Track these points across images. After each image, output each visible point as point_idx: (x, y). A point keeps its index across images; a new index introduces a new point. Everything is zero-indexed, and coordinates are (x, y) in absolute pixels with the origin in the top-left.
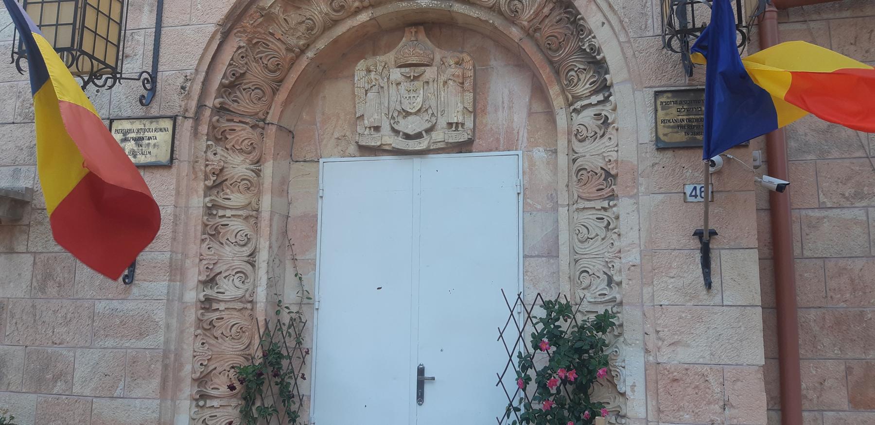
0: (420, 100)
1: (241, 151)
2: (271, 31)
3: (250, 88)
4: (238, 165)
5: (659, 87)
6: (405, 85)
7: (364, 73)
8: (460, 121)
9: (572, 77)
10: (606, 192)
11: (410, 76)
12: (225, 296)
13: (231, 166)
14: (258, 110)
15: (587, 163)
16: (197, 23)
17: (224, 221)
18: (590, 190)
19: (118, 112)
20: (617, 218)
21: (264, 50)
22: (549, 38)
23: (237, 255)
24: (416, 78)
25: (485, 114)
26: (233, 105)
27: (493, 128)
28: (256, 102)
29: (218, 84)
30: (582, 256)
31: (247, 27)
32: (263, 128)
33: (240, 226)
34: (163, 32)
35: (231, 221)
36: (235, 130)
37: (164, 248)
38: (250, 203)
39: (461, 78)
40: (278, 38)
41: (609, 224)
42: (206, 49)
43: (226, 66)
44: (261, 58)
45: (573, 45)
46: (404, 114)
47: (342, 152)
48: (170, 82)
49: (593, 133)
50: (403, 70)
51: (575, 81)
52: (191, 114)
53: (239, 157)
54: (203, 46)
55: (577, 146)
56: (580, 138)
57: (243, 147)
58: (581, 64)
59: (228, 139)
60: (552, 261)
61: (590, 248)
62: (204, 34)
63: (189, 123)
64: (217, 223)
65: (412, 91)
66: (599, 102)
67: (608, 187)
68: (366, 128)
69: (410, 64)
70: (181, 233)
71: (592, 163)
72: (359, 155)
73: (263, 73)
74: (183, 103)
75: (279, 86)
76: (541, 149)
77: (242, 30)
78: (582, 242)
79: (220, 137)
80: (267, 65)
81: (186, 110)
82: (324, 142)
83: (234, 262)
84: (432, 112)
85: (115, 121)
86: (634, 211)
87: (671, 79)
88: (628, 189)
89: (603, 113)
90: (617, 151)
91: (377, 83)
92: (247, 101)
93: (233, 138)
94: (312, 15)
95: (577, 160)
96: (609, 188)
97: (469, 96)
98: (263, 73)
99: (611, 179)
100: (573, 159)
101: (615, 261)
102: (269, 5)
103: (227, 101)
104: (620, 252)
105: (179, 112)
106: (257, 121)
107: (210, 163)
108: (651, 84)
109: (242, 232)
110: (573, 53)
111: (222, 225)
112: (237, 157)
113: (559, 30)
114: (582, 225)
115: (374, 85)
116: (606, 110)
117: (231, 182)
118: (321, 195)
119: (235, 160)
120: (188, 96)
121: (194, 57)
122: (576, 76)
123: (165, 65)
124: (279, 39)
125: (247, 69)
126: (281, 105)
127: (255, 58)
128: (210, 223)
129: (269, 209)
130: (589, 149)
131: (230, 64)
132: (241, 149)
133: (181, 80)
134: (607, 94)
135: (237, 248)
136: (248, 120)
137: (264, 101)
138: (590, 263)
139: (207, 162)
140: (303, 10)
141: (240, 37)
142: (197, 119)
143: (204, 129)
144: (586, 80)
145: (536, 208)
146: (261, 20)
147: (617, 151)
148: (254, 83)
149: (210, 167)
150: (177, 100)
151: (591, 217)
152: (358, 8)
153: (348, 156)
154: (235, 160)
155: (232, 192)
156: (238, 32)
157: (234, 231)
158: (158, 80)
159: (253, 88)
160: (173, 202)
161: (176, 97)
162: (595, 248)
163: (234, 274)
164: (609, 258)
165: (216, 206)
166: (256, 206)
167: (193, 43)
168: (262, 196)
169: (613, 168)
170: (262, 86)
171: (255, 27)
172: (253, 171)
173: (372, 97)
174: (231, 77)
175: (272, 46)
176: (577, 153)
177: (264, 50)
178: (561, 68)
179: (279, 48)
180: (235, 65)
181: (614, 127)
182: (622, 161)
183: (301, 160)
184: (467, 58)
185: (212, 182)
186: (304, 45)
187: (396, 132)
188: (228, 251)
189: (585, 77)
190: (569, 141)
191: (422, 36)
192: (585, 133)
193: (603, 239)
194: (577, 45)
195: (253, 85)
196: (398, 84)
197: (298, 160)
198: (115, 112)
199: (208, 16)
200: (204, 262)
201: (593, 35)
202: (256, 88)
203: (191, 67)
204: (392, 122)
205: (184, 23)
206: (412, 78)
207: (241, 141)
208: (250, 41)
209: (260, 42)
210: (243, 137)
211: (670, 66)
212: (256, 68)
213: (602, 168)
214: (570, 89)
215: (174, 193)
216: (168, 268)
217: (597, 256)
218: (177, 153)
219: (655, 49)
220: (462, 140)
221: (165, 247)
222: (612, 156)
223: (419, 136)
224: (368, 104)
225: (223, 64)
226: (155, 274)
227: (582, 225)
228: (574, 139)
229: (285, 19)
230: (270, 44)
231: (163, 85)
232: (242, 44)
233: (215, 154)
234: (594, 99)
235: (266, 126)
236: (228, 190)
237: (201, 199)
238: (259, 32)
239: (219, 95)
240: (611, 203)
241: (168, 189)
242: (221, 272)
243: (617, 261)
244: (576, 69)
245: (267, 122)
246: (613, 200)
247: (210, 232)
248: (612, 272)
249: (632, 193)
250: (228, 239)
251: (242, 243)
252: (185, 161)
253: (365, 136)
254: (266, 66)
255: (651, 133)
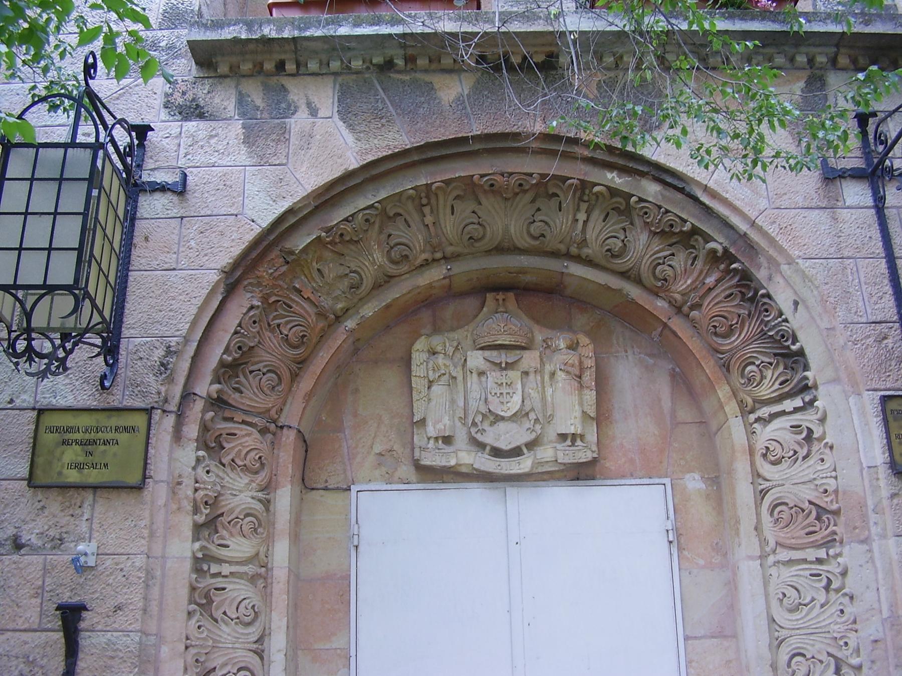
0: (517, 399)
1: (246, 469)
2: (297, 286)
3: (259, 370)
4: (240, 491)
5: (889, 390)
6: (493, 377)
7: (424, 356)
8: (579, 432)
9: (752, 374)
10: (820, 536)
11: (501, 363)
12: (811, 569)
13: (229, 492)
14: (270, 405)
15: (789, 495)
16: (188, 268)
17: (219, 582)
18: (797, 533)
19: (51, 399)
20: (844, 574)
21: (283, 313)
22: (716, 318)
23: (240, 640)
24: (509, 366)
25: (611, 423)
26: (233, 396)
27: (625, 444)
28: (268, 392)
29: (217, 362)
30: (793, 632)
31: (264, 277)
32: (274, 434)
33: (243, 592)
34: (131, 279)
35: (230, 582)
36: (235, 435)
37: (129, 625)
38: (257, 554)
39: (578, 368)
40: (306, 297)
41: (829, 582)
42: (202, 309)
43: (230, 335)
44: (279, 326)
45: (751, 329)
46: (492, 418)
47: (387, 475)
48: (141, 355)
49: (792, 453)
50: (487, 353)
51: (758, 378)
52: (173, 406)
53: (241, 478)
54: (199, 302)
55: (766, 469)
56: (773, 459)
57: (247, 462)
58: (766, 356)
59: (224, 448)
60: (726, 643)
61: (805, 620)
62: (200, 285)
63: (170, 420)
64: (208, 585)
65: (504, 384)
66: (796, 410)
67: (823, 529)
68: (429, 439)
69: (500, 345)
70: (155, 600)
71: (795, 495)
72: (415, 480)
73: (281, 347)
74: (163, 389)
75: (299, 369)
76: (697, 476)
77: (254, 281)
78: (791, 611)
79: (214, 445)
80: (287, 336)
81: (166, 401)
82: (358, 459)
83: (235, 652)
84: (535, 417)
85: (46, 413)
86: (868, 562)
87: (897, 380)
88: (857, 531)
89: (805, 424)
90: (836, 478)
91: (448, 371)
92: (256, 390)
93: (233, 448)
94: (359, 267)
95: (768, 491)
96: (826, 530)
97: (590, 396)
98: (281, 347)
99: (828, 518)
100: (761, 492)
101: (848, 635)
102: (301, 248)
103: (226, 389)
104: (855, 622)
105: (156, 402)
106: (268, 422)
107: (202, 486)
108: (874, 386)
109: (247, 601)
110: (753, 339)
111: (216, 589)
112: (239, 479)
113: (730, 307)
114: (788, 585)
115: (444, 374)
116: (807, 419)
117: (230, 519)
118: (356, 543)
119: (236, 484)
120: (170, 380)
121: (184, 318)
122: (758, 372)
123: (134, 328)
124: (308, 298)
125: (259, 342)
126: (304, 398)
127: (269, 325)
128: (199, 585)
129: (286, 564)
130: (788, 476)
131: (236, 333)
132: (245, 465)
133: (160, 352)
134: (807, 399)
135: (241, 629)
136: (255, 420)
137: (280, 392)
138: (806, 641)
139: (197, 485)
140: (347, 258)
141: (251, 292)
142: (180, 416)
143: (192, 430)
144: (773, 380)
145: (697, 564)
146: (284, 268)
147: (836, 478)
148: (268, 363)
149: (201, 493)
150: (154, 384)
151: (801, 573)
152: (427, 260)
153: (398, 483)
154: (236, 484)
155: (232, 535)
156: (250, 284)
157: (234, 599)
158: (121, 352)
159: (265, 370)
160: (145, 549)
161: (151, 379)
162: (812, 619)
163: (235, 671)
164: (839, 632)
165: (209, 558)
166: (265, 558)
167: (181, 297)
168: (274, 541)
169: (832, 501)
170: (278, 368)
171: (275, 279)
172: (260, 501)
173: (440, 392)
174: (236, 352)
175: (297, 308)
176: (768, 480)
177: (283, 313)
178: (734, 360)
179: (307, 312)
180: (243, 333)
181: (827, 443)
182: (844, 493)
183: (319, 486)
184: (584, 340)
185: (204, 517)
186: (342, 309)
187: (481, 446)
188: (227, 632)
189: (773, 375)
190: (752, 464)
191: (512, 303)
192: (779, 452)
193: (822, 606)
194: (757, 329)
195: (265, 366)
196: (481, 374)
197: (314, 486)
198: (44, 398)
199: (207, 258)
200: (193, 651)
201: (783, 317)
202: (269, 371)
203: (178, 333)
204: (473, 430)
205: (166, 266)
206: (503, 365)
207: (244, 452)
208: (265, 299)
209: (279, 301)
210: (247, 446)
211: (893, 363)
212: (272, 341)
213: (810, 503)
214: (751, 390)
215: (146, 533)
216: (136, 659)
217: (817, 631)
218: (152, 467)
219: (872, 339)
220: (585, 460)
221: (131, 624)
222: (828, 484)
223: (516, 452)
224: (433, 403)
225: (226, 331)
226: (113, 669)
227: (788, 585)
228: (759, 460)
229: (319, 270)
230: (294, 306)
231: (129, 359)
232: (256, 303)
233: (208, 472)
234: (788, 405)
235: (279, 431)
236: (225, 532)
237: (188, 544)
238: (280, 286)
239: (217, 380)
240: (831, 552)
241: (135, 526)
242: (215, 668)
243: (852, 635)
244: (757, 363)
245: (280, 424)
246: (832, 547)
247: (198, 601)
248: (845, 652)
249: (862, 537)
250: (225, 613)
251: (247, 619)
252: (162, 481)
253: (429, 450)
254: (286, 339)
255: (884, 453)
